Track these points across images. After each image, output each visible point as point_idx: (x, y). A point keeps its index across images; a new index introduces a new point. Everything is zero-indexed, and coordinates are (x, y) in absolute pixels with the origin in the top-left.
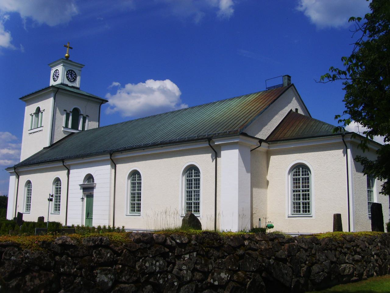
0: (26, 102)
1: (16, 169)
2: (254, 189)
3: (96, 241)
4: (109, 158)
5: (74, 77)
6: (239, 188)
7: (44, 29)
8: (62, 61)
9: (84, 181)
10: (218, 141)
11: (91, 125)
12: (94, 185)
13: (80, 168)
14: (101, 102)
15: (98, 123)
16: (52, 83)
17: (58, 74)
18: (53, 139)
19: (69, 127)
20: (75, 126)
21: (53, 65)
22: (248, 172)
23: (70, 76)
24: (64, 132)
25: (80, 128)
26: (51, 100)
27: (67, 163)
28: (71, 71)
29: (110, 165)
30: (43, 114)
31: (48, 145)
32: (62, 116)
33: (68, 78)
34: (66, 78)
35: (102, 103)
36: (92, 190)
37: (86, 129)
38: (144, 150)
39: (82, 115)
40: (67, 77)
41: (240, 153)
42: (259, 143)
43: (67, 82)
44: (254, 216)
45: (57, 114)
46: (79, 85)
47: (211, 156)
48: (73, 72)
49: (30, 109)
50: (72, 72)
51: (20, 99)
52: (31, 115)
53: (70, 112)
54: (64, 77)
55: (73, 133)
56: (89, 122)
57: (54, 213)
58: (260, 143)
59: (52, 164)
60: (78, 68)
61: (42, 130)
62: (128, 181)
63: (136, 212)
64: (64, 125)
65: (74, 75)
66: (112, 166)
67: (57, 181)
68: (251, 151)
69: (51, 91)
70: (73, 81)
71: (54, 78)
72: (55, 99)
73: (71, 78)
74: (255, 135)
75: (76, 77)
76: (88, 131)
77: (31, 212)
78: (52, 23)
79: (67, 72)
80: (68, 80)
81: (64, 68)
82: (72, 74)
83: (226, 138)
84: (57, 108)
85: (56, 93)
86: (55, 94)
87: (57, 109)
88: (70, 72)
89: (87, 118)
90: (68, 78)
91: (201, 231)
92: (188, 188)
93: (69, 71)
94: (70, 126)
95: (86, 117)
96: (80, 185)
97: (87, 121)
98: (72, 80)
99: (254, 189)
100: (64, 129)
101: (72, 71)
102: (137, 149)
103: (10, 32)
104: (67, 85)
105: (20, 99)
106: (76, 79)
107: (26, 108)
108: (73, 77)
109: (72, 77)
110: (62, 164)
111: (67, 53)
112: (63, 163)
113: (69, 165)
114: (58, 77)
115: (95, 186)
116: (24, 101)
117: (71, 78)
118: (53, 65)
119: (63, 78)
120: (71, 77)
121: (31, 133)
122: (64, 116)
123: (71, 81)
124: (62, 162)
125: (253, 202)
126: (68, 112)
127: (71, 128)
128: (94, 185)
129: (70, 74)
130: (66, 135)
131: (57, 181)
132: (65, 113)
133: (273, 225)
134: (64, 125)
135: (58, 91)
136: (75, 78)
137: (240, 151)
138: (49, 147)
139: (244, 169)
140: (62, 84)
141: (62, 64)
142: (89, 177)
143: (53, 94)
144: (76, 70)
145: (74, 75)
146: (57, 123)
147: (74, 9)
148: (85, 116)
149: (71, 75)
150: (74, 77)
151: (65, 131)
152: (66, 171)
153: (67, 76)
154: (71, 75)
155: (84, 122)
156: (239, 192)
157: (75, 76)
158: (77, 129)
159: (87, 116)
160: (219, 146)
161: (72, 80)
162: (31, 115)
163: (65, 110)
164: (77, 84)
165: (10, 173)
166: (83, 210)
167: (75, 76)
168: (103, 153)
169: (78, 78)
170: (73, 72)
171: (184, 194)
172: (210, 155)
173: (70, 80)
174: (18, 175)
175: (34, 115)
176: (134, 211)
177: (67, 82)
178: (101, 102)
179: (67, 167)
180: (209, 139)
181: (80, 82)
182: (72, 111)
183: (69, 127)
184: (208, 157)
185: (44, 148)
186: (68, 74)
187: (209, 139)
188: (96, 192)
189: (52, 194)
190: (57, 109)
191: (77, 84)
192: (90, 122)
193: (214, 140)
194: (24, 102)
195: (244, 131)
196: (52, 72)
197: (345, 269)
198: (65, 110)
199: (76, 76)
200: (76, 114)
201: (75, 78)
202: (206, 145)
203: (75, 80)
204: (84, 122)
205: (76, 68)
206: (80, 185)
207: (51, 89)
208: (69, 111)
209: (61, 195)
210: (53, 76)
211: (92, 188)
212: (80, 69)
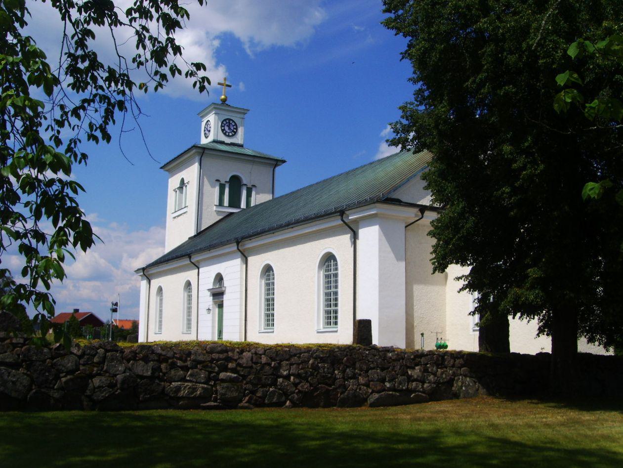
0: (169, 172)
1: (145, 270)
2: (417, 289)
3: (474, 381)
4: (235, 248)
5: (234, 129)
6: (380, 285)
7: (275, 54)
8: (213, 107)
9: (214, 283)
10: (354, 213)
11: (259, 198)
12: (223, 289)
13: (210, 265)
14: (275, 163)
15: (271, 195)
16: (204, 141)
17: (210, 127)
18: (201, 224)
19: (225, 205)
20: (235, 201)
21: (204, 113)
22: (398, 259)
23: (227, 128)
24: (218, 212)
25: (243, 205)
26: (196, 167)
27: (195, 259)
28: (227, 121)
29: (240, 259)
30: (188, 188)
31: (193, 234)
32: (213, 189)
33: (224, 132)
34: (221, 132)
35: (276, 166)
36: (222, 296)
37: (253, 203)
38: (273, 233)
39: (245, 185)
40: (223, 130)
41: (382, 230)
42: (420, 214)
43: (222, 138)
44: (415, 330)
45: (205, 187)
46: (242, 141)
47: (349, 237)
48: (231, 122)
49: (174, 182)
50: (229, 123)
51: (161, 168)
52: (174, 190)
53: (226, 182)
54: (218, 132)
55: (231, 214)
56: (257, 196)
57: (265, 331)
58: (421, 212)
59: (181, 261)
60: (239, 115)
61: (187, 212)
62: (260, 282)
63: (332, 326)
64: (217, 203)
65: (233, 126)
66: (242, 259)
67: (329, 260)
68: (406, 227)
69: (194, 154)
70: (233, 135)
71: (205, 134)
72: (200, 165)
73: (229, 131)
74: (419, 200)
75: (237, 129)
76: (256, 206)
77: (162, 332)
78: (288, 40)
79: (222, 123)
80: (225, 134)
81: (217, 117)
82: (229, 125)
83: (359, 209)
84: (205, 177)
85: (202, 156)
86: (200, 157)
87: (205, 179)
88: (227, 123)
89: (254, 189)
90: (224, 132)
91: (136, 345)
92: (328, 288)
93: (225, 120)
94: (226, 203)
95: (251, 188)
96: (209, 290)
97: (253, 193)
98: (231, 134)
99: (417, 289)
100: (216, 208)
101: (230, 120)
102: (267, 233)
103: (221, 64)
104: (222, 143)
105: (161, 168)
106: (237, 131)
107: (170, 180)
108: (232, 128)
109: (229, 129)
110: (189, 260)
111: (223, 93)
112: (190, 257)
113: (198, 262)
114: (209, 131)
115: (225, 291)
116: (167, 171)
117: (229, 131)
118: (204, 113)
119: (216, 133)
120: (229, 129)
121: (175, 218)
122: (217, 189)
123: (228, 136)
124: (188, 259)
125: (415, 308)
126: (223, 182)
127: (228, 206)
128: (223, 289)
129: (227, 126)
130: (221, 217)
131: (329, 260)
132: (218, 184)
133: (447, 344)
134: (217, 202)
135: (204, 152)
136: (235, 130)
137: (383, 229)
138: (195, 236)
139: (392, 255)
140: (214, 141)
141: (214, 112)
142: (219, 278)
143: (197, 158)
144: (236, 118)
145: (233, 126)
146: (206, 200)
147: (318, 16)
148: (249, 186)
149: (229, 126)
150: (234, 129)
151: (219, 211)
152: (197, 270)
153: (223, 128)
154: (229, 126)
155: (249, 196)
156: (380, 291)
157: (235, 127)
158: (238, 206)
159: (254, 186)
160: (356, 221)
161: (231, 134)
162: (174, 190)
163: (217, 180)
164: (239, 139)
165: (141, 277)
166: (213, 327)
167: (235, 127)
168: (227, 243)
169: (241, 131)
170: (231, 122)
171: (322, 298)
172: (349, 235)
173: (227, 134)
174: (148, 279)
175: (178, 191)
176: (330, 324)
177: (222, 138)
178: (275, 163)
179: (196, 264)
180: (342, 213)
181: (243, 135)
182: (228, 180)
183: (225, 205)
184: (346, 238)
185: (190, 238)
186: (223, 125)
187: (342, 213)
188: (226, 298)
189: (114, 302)
190: (205, 179)
191: (239, 139)
192: (258, 194)
193: (347, 212)
194: (167, 173)
195: (395, 196)
196: (203, 124)
197: (178, 389)
198: (217, 180)
199: (237, 126)
200: (235, 183)
201: (235, 130)
202: (338, 222)
203: (235, 133)
204: (249, 196)
205: (236, 115)
206: (209, 290)
207: (194, 151)
208: (224, 181)
209: (339, 308)
210: (205, 131)
211: (221, 294)
212: (242, 116)
